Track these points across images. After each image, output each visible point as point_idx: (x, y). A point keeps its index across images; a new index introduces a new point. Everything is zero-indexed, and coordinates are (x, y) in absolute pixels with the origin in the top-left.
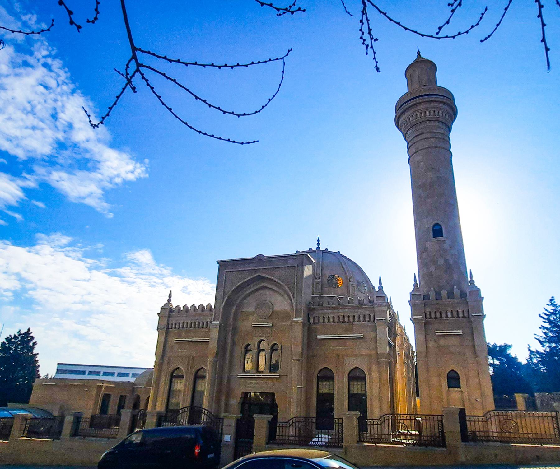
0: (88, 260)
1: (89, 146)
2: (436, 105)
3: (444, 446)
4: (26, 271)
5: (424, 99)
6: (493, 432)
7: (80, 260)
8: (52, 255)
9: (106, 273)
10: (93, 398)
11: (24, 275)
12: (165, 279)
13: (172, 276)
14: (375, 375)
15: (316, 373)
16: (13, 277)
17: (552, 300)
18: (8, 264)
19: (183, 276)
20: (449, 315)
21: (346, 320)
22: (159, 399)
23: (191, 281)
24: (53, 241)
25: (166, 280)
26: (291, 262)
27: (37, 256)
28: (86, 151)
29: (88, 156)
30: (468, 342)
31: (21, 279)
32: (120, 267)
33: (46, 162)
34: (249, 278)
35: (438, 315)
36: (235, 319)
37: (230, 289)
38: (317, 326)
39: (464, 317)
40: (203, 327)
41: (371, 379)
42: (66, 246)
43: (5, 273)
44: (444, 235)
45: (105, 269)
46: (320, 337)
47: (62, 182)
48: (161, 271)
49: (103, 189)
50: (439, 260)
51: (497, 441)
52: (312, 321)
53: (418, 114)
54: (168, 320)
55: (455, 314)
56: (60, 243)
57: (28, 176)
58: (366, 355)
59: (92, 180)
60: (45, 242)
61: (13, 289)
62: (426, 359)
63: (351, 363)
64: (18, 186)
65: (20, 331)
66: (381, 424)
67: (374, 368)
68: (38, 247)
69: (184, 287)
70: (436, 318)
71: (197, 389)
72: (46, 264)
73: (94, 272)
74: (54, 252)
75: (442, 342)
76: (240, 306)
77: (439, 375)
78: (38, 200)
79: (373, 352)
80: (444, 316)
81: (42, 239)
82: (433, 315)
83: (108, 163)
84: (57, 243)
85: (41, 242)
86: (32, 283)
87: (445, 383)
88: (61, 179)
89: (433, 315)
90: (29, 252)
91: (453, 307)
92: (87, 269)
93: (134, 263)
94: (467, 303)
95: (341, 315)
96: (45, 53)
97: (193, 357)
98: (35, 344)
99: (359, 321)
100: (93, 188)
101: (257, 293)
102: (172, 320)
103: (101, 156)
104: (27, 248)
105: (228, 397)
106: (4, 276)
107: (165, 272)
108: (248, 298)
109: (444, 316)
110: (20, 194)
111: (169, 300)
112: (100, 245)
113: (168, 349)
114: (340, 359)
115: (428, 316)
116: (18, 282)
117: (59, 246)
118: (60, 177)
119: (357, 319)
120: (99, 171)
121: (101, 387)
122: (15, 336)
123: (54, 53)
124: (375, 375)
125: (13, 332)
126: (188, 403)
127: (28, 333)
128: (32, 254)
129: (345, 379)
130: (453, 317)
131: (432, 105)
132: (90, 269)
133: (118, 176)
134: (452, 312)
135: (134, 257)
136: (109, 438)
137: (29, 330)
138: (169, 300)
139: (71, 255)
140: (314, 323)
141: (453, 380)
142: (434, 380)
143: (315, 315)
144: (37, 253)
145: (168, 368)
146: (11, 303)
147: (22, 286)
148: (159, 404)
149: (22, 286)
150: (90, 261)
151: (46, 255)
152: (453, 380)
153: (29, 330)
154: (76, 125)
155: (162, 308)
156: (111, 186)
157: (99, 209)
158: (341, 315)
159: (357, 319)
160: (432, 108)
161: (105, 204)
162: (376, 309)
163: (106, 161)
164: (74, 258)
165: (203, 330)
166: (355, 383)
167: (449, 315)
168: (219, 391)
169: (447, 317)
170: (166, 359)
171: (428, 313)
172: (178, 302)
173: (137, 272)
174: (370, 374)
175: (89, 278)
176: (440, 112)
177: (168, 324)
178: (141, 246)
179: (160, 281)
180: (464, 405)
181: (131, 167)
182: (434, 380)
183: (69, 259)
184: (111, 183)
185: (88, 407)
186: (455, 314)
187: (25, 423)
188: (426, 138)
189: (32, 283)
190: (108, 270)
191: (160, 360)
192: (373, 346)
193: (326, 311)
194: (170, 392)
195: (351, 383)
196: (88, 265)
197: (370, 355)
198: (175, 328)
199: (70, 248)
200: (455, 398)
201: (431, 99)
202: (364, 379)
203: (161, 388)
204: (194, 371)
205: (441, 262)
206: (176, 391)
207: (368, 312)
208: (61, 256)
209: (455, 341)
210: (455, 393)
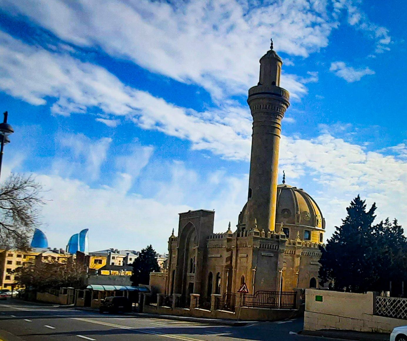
9: (380, 153)
11: (309, 164)
16: (300, 167)
18: (295, 157)
27: (320, 146)
28: (360, 33)
43: (293, 164)
46: (209, 256)
47: (339, 72)
60: (326, 131)
68: (321, 138)
72: (327, 152)
76: (189, 239)
85: (322, 131)
86: (315, 170)
90: (313, 143)
92: (362, 151)
104: (312, 140)
105: (185, 286)
106: (293, 167)
111: (173, 234)
128: (315, 144)
132: (366, 151)
137: (151, 246)
138: (173, 234)
150: (366, 144)
153: (151, 246)
154: (351, 10)
170: (171, 265)
175: (365, 159)
182: (237, 280)
183: (346, 144)
189: (315, 170)
208: (340, 141)
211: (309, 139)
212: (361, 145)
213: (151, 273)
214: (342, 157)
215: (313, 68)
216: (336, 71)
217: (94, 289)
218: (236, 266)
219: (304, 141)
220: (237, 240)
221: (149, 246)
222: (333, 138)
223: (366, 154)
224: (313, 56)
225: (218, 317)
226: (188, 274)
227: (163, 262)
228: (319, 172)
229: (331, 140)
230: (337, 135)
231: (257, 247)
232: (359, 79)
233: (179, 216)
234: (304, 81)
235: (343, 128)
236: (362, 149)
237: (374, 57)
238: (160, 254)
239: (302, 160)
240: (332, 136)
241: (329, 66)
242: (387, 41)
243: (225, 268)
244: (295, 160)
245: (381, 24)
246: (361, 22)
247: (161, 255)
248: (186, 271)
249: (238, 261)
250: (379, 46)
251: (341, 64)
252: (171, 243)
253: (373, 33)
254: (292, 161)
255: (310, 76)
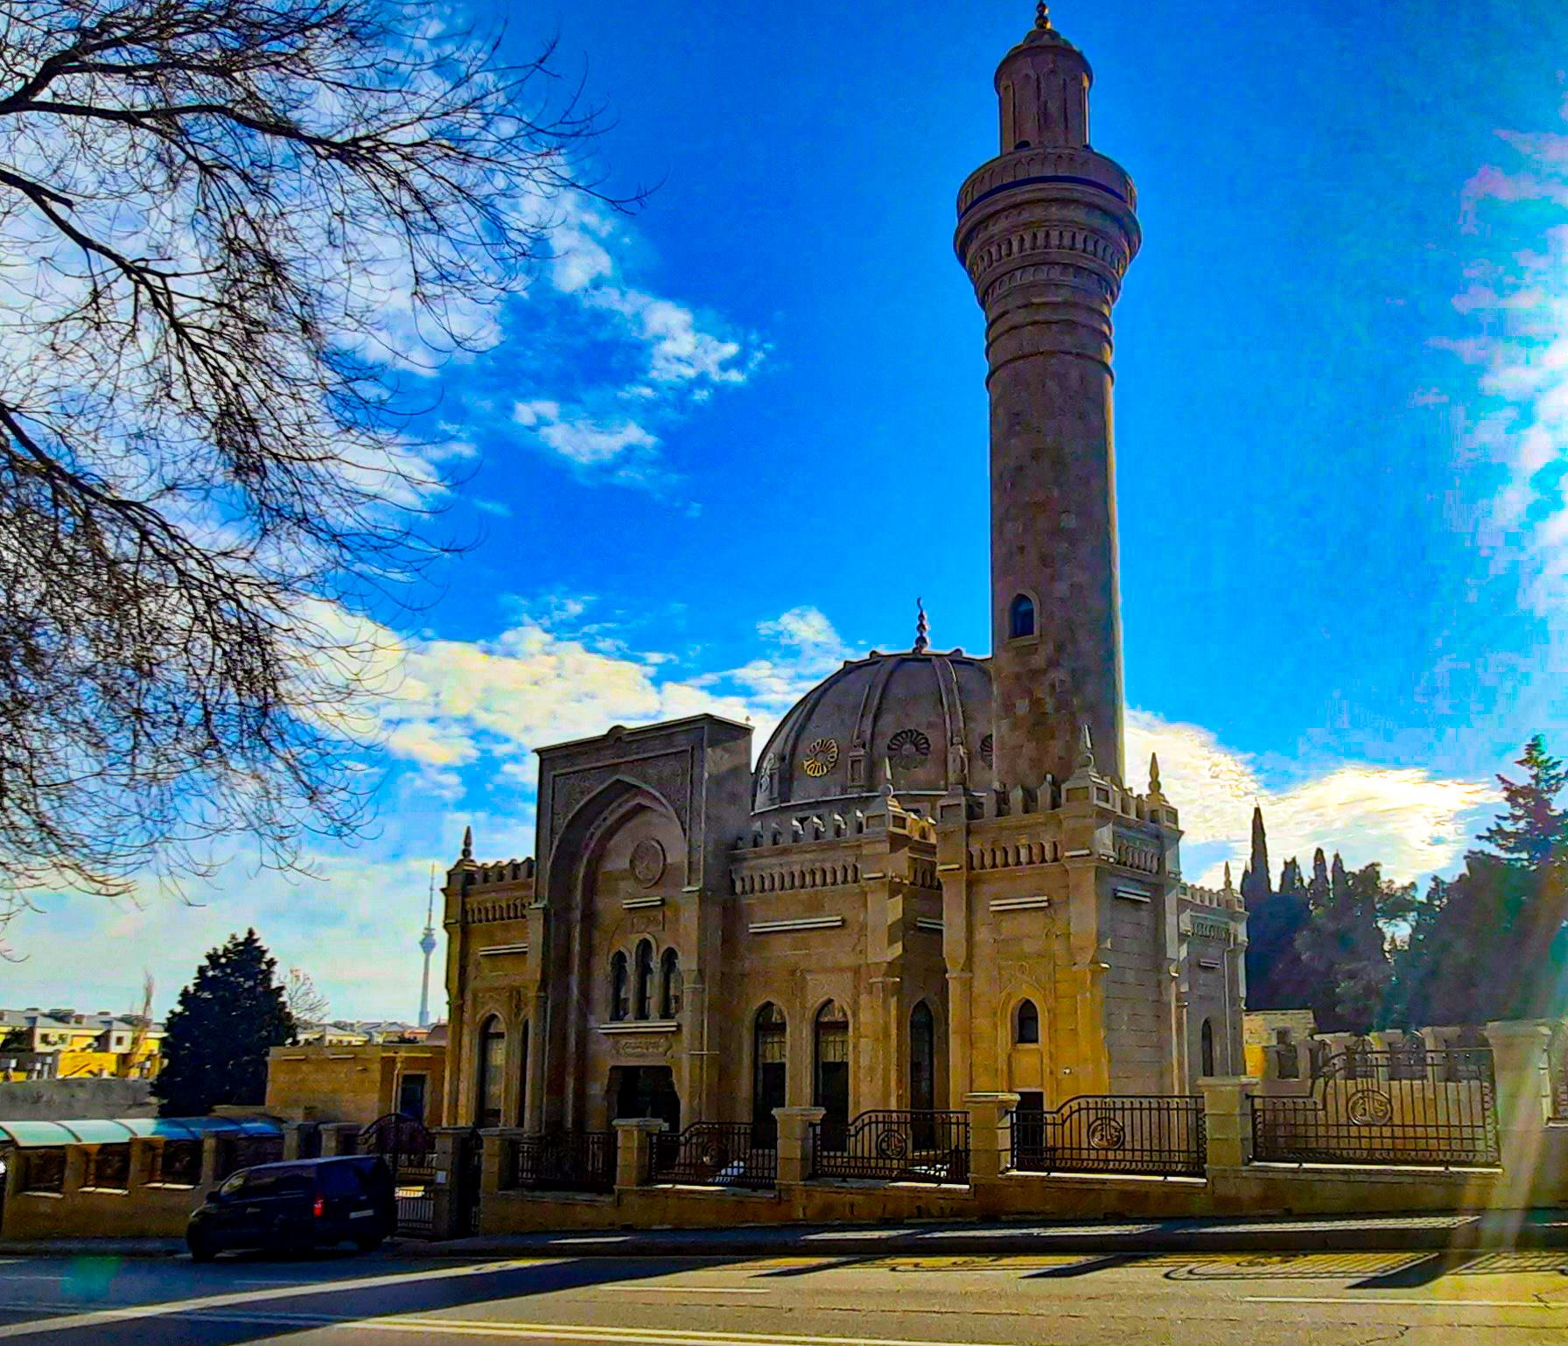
0: (647, 654)
1: (609, 299)
2: (1038, 213)
4: (487, 710)
5: (1001, 200)
7: (624, 657)
8: (549, 654)
9: (703, 688)
11: (484, 720)
16: (456, 730)
17: (1533, 746)
18: (437, 695)
24: (546, 611)
26: (682, 743)
27: (512, 662)
28: (600, 318)
29: (604, 335)
31: (478, 734)
32: (742, 663)
33: (492, 374)
34: (601, 788)
37: (562, 822)
38: (745, 900)
42: (582, 620)
43: (432, 720)
44: (1036, 631)
45: (697, 674)
46: (754, 927)
47: (545, 430)
49: (662, 431)
50: (1018, 703)
52: (738, 888)
53: (993, 250)
54: (464, 903)
56: (564, 615)
57: (451, 428)
58: (849, 969)
59: (626, 408)
60: (526, 618)
61: (459, 763)
63: (820, 989)
64: (431, 462)
65: (233, 937)
66: (1063, 1124)
68: (509, 636)
72: (536, 683)
73: (669, 687)
74: (552, 644)
76: (599, 856)
78: (490, 497)
81: (514, 611)
82: (988, 860)
83: (668, 347)
84: (557, 615)
85: (515, 619)
86: (507, 740)
88: (542, 421)
89: (988, 860)
90: (489, 652)
91: (1031, 836)
92: (648, 683)
93: (777, 646)
95: (796, 869)
96: (434, 28)
98: (271, 963)
100: (633, 434)
101: (630, 825)
102: (473, 902)
103: (642, 326)
104: (482, 642)
105: (582, 1079)
106: (430, 730)
108: (616, 838)
110: (435, 487)
111: (466, 853)
112: (677, 607)
114: (796, 978)
115: (976, 862)
116: (468, 742)
117: (563, 623)
118: (539, 417)
120: (643, 377)
121: (393, 1060)
122: (226, 949)
123: (460, 21)
124: (864, 1016)
125: (220, 942)
127: (251, 938)
128: (495, 658)
129: (807, 1032)
130: (1031, 862)
131: (1026, 216)
132: (657, 682)
133: (702, 381)
134: (1030, 848)
135: (780, 628)
137: (251, 933)
138: (466, 853)
139: (601, 645)
140: (744, 892)
143: (746, 873)
144: (510, 654)
146: (461, 806)
147: (483, 751)
149: (483, 751)
150: (656, 658)
151: (532, 655)
152: (1026, 1024)
153: (251, 933)
154: (560, 241)
155: (449, 874)
156: (683, 418)
157: (658, 496)
158: (796, 869)
160: (1027, 225)
161: (674, 478)
163: (660, 338)
164: (608, 655)
170: (469, 996)
171: (976, 854)
172: (484, 857)
173: (790, 672)
174: (855, 1015)
175: (657, 706)
176: (1054, 234)
178: (791, 596)
181: (731, 349)
182: (982, 1024)
183: (596, 659)
184: (683, 410)
187: (150, 1155)
188: (1012, 328)
189: (507, 740)
190: (710, 678)
193: (763, 861)
195: (822, 1038)
196: (651, 671)
199: (595, 627)
201: (1019, 199)
203: (465, 1066)
208: (573, 652)
211: (472, 640)
212: (638, 660)
213: (273, 1050)
214: (587, 701)
215: (459, 414)
216: (532, 429)
217: (22, 1143)
218: (969, 964)
219: (456, 647)
220: (968, 833)
221: (241, 937)
222: (548, 638)
223: (660, 692)
224: (451, 376)
225: (1297, 1207)
226: (601, 1025)
227: (90, 1040)
228: (520, 746)
229: (545, 645)
230: (564, 630)
231: (233, 1010)
232: (607, 457)
233: (536, 759)
234: (436, 453)
235: (575, 608)
236: (645, 676)
237: (647, 392)
238: (78, 1012)
239: (460, 707)
240: (546, 631)
241: (508, 409)
242: (685, 343)
243: (886, 975)
244: (437, 705)
245: (669, 288)
246: (597, 283)
247: (81, 1017)
248: (584, 1016)
249: (983, 934)
250: (661, 364)
251: (548, 408)
252: (465, 895)
253: (639, 320)
254: (430, 711)
255: (448, 438)
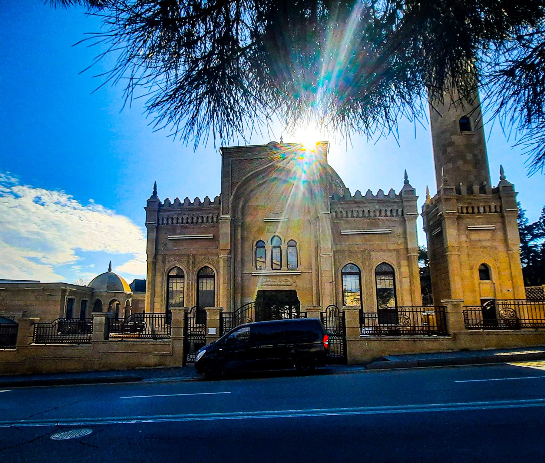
3: (446, 334)
6: (525, 320)
10: (59, 303)
12: (13, 188)
13: (22, 186)
14: (405, 270)
15: (374, 268)
19: (35, 186)
20: (482, 210)
21: (372, 214)
22: (157, 300)
23: (44, 191)
25: (15, 189)
30: (500, 235)
35: (470, 210)
36: (243, 215)
39: (496, 212)
40: (202, 222)
41: (400, 274)
48: (9, 179)
51: (530, 328)
55: (487, 209)
58: (395, 250)
62: (408, 255)
67: (404, 263)
69: (37, 197)
70: (467, 213)
71: (200, 289)
75: (474, 236)
77: (471, 268)
79: (402, 247)
80: (476, 211)
87: (477, 275)
94: (500, 198)
97: (194, 256)
99: (386, 215)
107: (13, 180)
109: (476, 211)
111: (155, 193)
113: (161, 248)
119: (383, 214)
126: (194, 304)
130: (485, 212)
134: (484, 207)
136: (79, 343)
138: (155, 193)
141: (485, 273)
142: (467, 273)
145: (164, 267)
148: (157, 305)
152: (485, 273)
159: (383, 214)
162: (405, 204)
165: (202, 225)
166: (205, 281)
167: (482, 210)
168: (235, 290)
169: (479, 212)
170: (160, 258)
174: (399, 269)
177: (158, 219)
179: (8, 190)
180: (495, 295)
185: (53, 312)
186: (487, 209)
191: (153, 259)
192: (402, 240)
194: (169, 294)
197: (398, 251)
198: (167, 223)
200: (485, 290)
202: (213, 276)
204: (196, 269)
205: (469, 157)
206: (172, 291)
207: (395, 207)
209: (488, 235)
210: (486, 285)
